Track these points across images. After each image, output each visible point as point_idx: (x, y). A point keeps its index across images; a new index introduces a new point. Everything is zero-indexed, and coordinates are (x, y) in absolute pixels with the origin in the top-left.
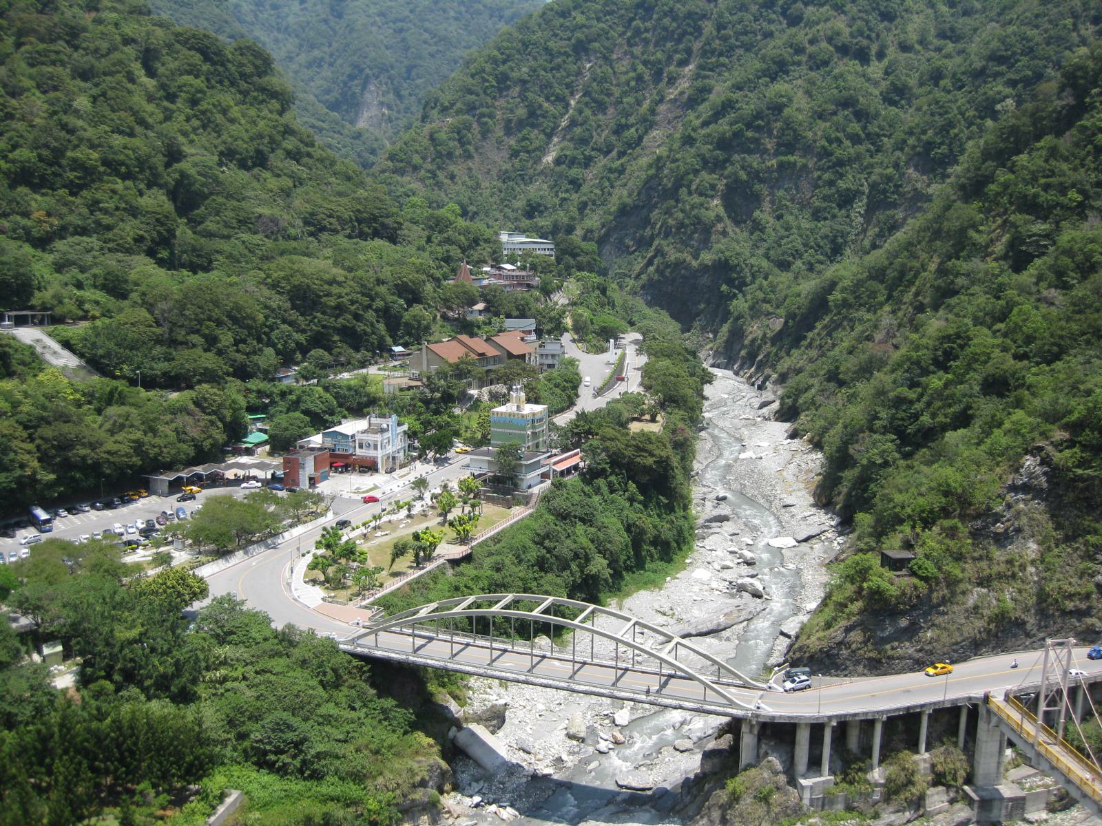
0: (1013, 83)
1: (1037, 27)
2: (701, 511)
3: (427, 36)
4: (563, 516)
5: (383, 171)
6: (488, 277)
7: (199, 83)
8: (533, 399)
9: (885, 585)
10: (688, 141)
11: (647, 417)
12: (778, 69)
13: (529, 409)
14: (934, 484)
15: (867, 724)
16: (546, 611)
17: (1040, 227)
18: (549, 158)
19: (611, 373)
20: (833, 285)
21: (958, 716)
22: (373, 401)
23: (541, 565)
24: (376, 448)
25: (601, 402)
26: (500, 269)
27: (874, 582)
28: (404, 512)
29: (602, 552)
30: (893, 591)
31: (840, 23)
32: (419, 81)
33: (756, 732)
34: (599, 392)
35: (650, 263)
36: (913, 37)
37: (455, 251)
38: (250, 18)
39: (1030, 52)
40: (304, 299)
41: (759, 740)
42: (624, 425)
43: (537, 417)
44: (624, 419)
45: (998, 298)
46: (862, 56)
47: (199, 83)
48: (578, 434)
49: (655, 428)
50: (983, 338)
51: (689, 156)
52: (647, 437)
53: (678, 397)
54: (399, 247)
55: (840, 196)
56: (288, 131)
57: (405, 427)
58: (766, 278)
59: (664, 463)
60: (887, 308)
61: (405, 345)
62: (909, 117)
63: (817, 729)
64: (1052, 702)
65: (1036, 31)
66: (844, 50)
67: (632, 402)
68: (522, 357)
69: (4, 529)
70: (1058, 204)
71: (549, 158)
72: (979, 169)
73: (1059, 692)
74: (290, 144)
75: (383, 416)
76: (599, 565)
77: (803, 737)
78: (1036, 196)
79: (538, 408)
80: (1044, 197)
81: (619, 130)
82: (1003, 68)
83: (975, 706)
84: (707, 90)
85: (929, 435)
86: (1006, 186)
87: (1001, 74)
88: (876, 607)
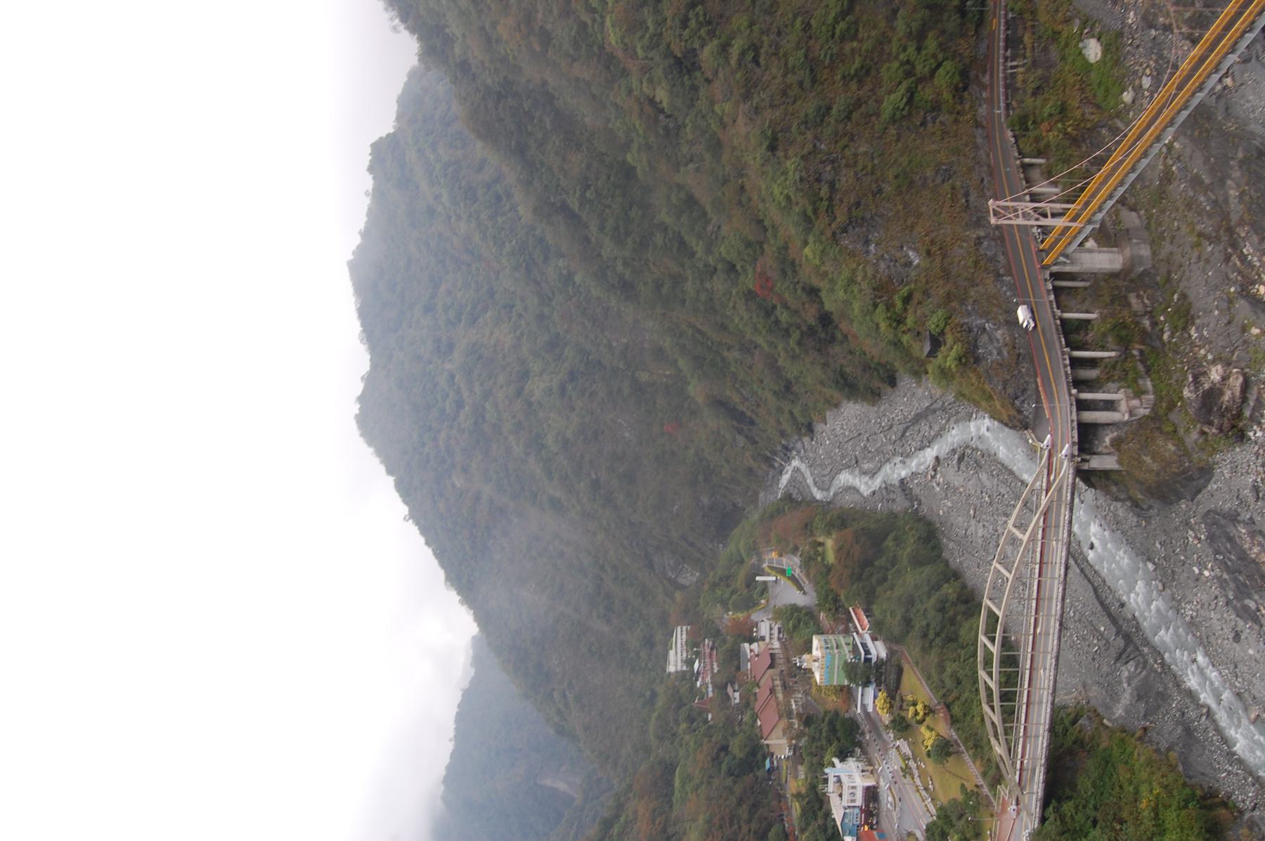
0: (546, 259)
4: (908, 622)
6: (705, 684)
8: (808, 649)
9: (953, 354)
11: (820, 549)
13: (816, 652)
14: (926, 589)
16: (992, 640)
21: (1062, 288)
22: (813, 788)
23: (952, 639)
24: (854, 787)
25: (807, 586)
26: (698, 673)
27: (950, 363)
28: (912, 764)
29: (938, 587)
30: (957, 348)
33: (1087, 457)
37: (684, 712)
41: (1094, 454)
42: (829, 569)
43: (823, 645)
44: (824, 570)
45: (716, 269)
48: (837, 610)
49: (830, 543)
50: (749, 281)
52: (839, 550)
53: (805, 517)
57: (836, 760)
58: (703, 450)
60: (725, 353)
61: (764, 758)
67: (807, 562)
72: (613, 286)
75: (826, 781)
76: (949, 590)
77: (1089, 416)
79: (816, 642)
85: (825, 319)
86: (625, 264)
88: (972, 360)
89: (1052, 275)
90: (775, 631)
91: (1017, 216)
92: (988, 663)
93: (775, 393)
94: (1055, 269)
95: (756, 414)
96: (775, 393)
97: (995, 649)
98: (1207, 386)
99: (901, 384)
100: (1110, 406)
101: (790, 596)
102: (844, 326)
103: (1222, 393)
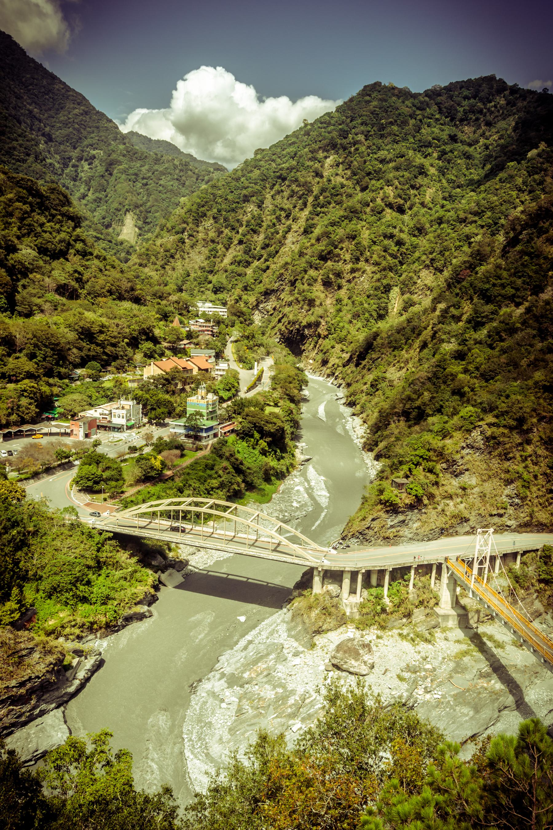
1: (496, 195)
2: (299, 456)
3: (161, 188)
5: (134, 265)
7: (27, 208)
10: (301, 254)
12: (354, 214)
15: (381, 573)
17: (489, 308)
18: (227, 261)
19: (259, 377)
20: (376, 335)
31: (390, 191)
32: (157, 214)
33: (321, 574)
34: (249, 390)
35: (279, 321)
36: (428, 199)
38: (60, 171)
39: (492, 209)
40: (87, 334)
46: (401, 210)
47: (27, 208)
49: (277, 410)
51: (302, 263)
54: (143, 308)
55: (384, 287)
56: (78, 239)
59: (282, 430)
62: (423, 242)
63: (354, 575)
64: (481, 563)
65: (496, 198)
66: (390, 206)
68: (207, 370)
69: (0, 429)
70: (500, 295)
71: (227, 261)
73: (485, 558)
74: (79, 246)
78: (487, 290)
80: (497, 290)
81: (266, 246)
82: (476, 218)
83: (441, 564)
84: (313, 226)
87: (475, 222)
89: (441, 564)
90: (221, 373)
91: (481, 546)
92: (197, 504)
93: (541, 438)
94: (444, 566)
95: (364, 368)
96: (541, 438)
97: (204, 510)
98: (361, 652)
99: (376, 463)
100: (353, 591)
101: (460, 368)
102: (417, 428)
103: (357, 660)
